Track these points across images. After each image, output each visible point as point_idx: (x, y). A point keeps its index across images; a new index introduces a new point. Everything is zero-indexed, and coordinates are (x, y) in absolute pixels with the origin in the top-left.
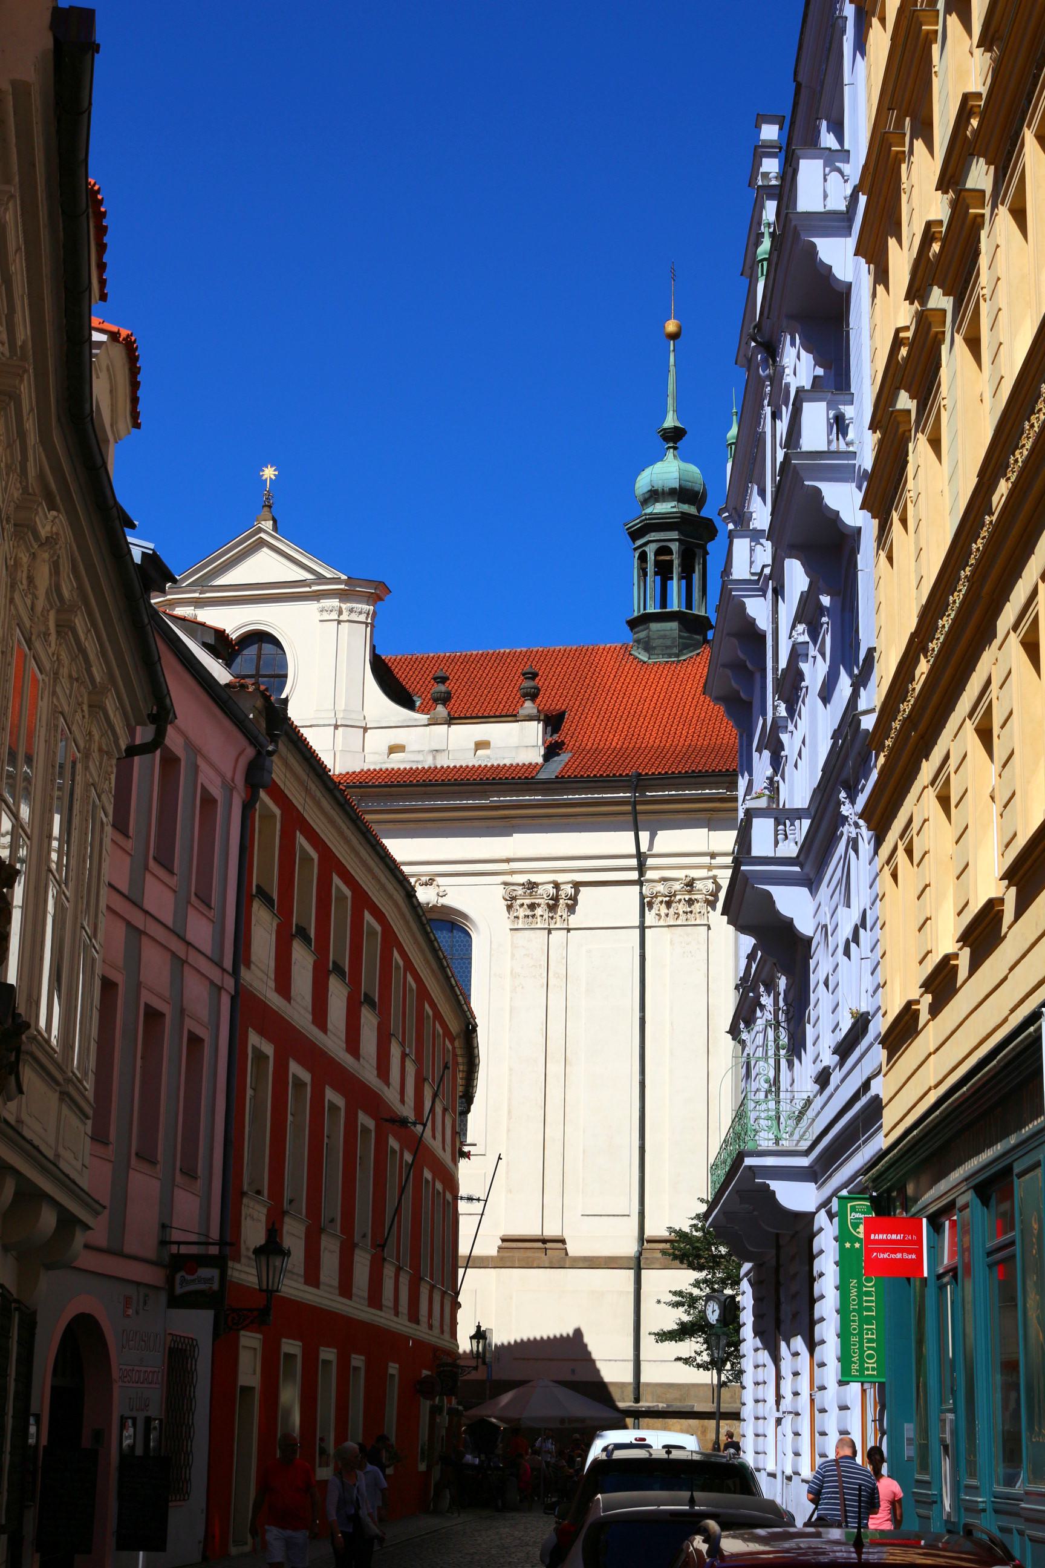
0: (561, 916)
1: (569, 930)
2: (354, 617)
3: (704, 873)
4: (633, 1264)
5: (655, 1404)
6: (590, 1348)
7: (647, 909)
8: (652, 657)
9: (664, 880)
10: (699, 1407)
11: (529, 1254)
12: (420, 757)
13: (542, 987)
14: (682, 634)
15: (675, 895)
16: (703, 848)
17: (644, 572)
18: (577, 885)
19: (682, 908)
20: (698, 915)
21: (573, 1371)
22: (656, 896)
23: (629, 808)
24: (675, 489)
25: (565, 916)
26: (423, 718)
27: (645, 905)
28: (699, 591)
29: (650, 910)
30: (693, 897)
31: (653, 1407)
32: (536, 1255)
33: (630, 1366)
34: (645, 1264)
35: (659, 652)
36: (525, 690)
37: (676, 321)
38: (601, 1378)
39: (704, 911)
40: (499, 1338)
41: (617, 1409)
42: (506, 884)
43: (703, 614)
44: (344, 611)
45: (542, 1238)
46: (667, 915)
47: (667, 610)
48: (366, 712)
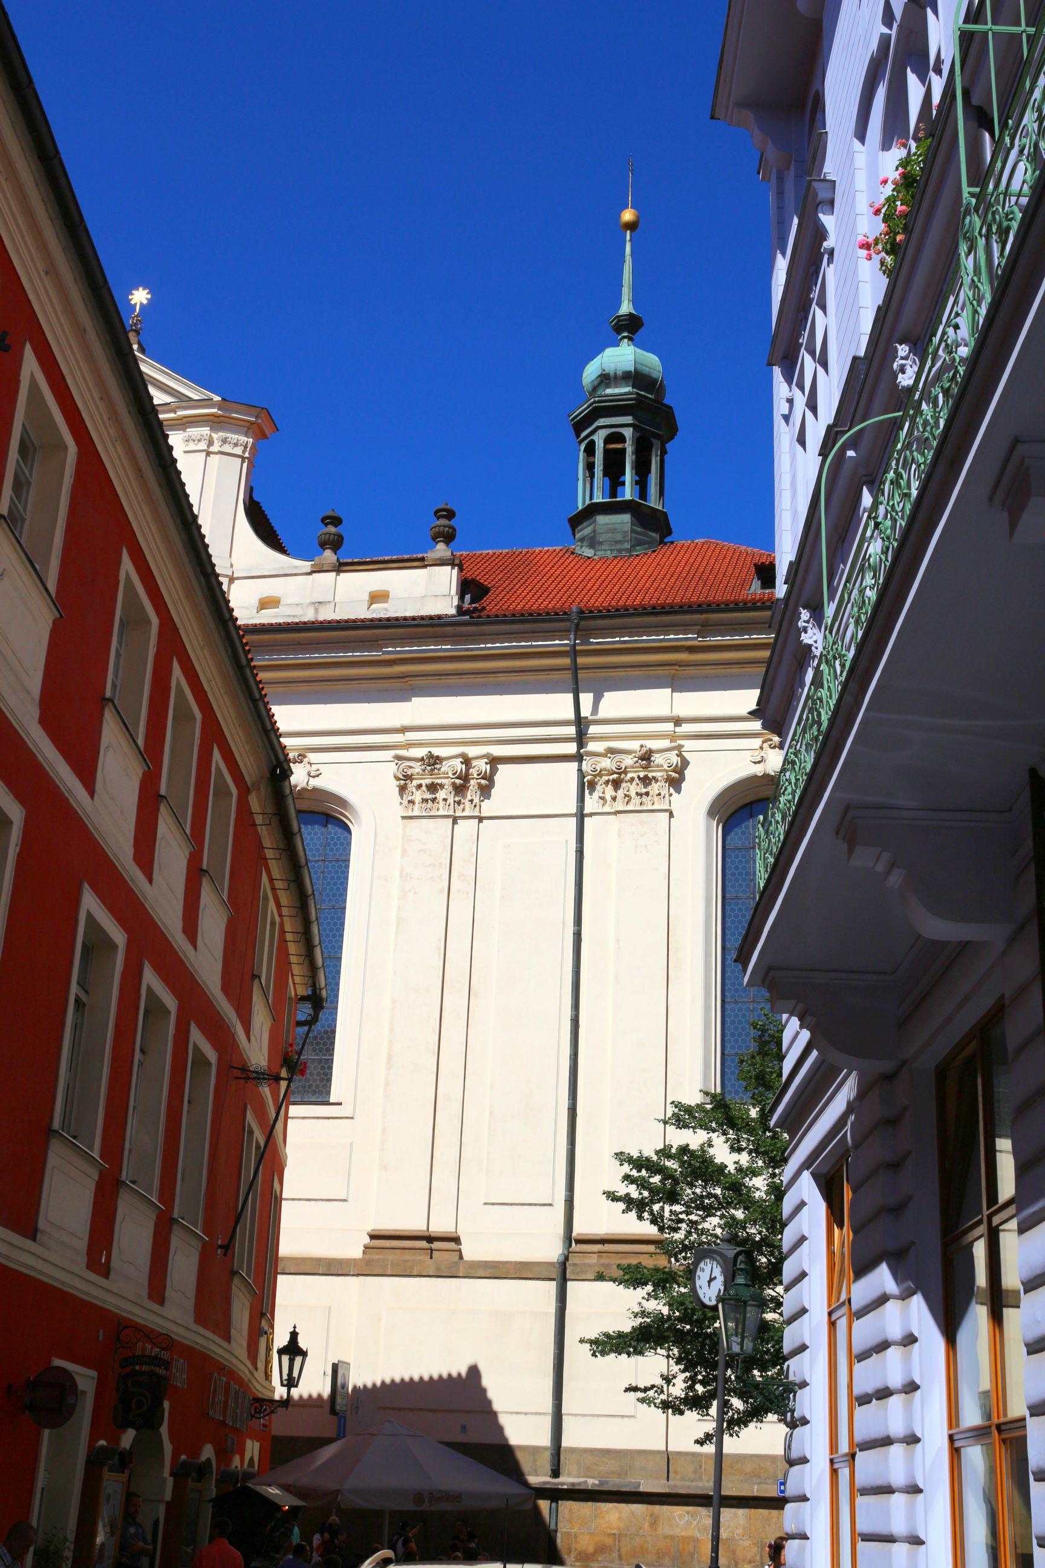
0: (471, 801)
1: (481, 819)
2: (227, 448)
3: (665, 743)
4: (555, 1273)
5: (581, 1480)
6: (491, 1394)
7: (587, 791)
8: (597, 553)
9: (612, 751)
10: (646, 1487)
11: (408, 1256)
12: (298, 611)
13: (442, 892)
14: (635, 528)
15: (625, 772)
16: (665, 712)
17: (590, 467)
18: (495, 761)
19: (634, 788)
20: (656, 799)
21: (464, 1428)
22: (600, 775)
23: (566, 661)
24: (630, 372)
25: (476, 800)
26: (306, 566)
27: (585, 785)
28: (656, 485)
29: (591, 793)
30: (650, 775)
31: (580, 1484)
32: (418, 1258)
33: (547, 1422)
34: (573, 1272)
35: (607, 548)
36: (437, 529)
37: (633, 210)
38: (506, 1440)
39: (664, 792)
40: (359, 1377)
41: (526, 1484)
42: (398, 758)
43: (661, 508)
44: (216, 442)
45: (426, 1234)
46: (614, 799)
47: (618, 499)
48: (234, 560)
